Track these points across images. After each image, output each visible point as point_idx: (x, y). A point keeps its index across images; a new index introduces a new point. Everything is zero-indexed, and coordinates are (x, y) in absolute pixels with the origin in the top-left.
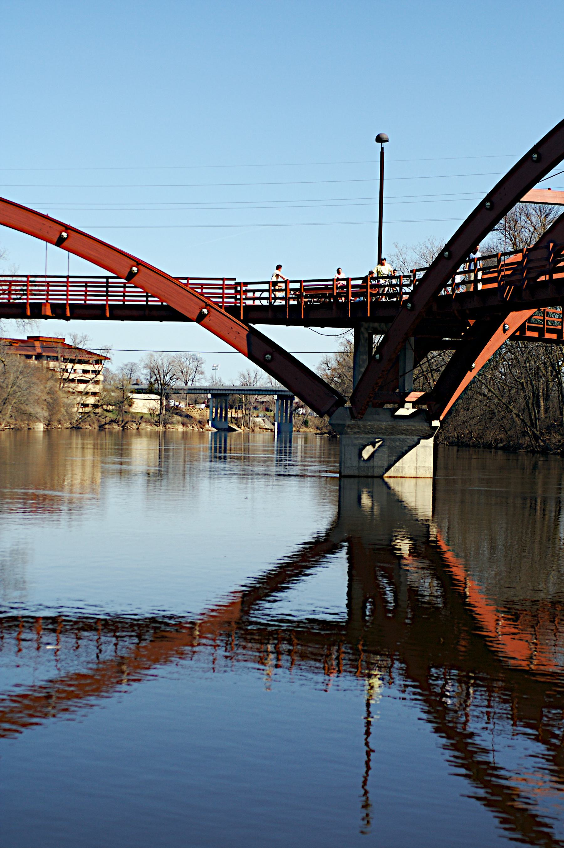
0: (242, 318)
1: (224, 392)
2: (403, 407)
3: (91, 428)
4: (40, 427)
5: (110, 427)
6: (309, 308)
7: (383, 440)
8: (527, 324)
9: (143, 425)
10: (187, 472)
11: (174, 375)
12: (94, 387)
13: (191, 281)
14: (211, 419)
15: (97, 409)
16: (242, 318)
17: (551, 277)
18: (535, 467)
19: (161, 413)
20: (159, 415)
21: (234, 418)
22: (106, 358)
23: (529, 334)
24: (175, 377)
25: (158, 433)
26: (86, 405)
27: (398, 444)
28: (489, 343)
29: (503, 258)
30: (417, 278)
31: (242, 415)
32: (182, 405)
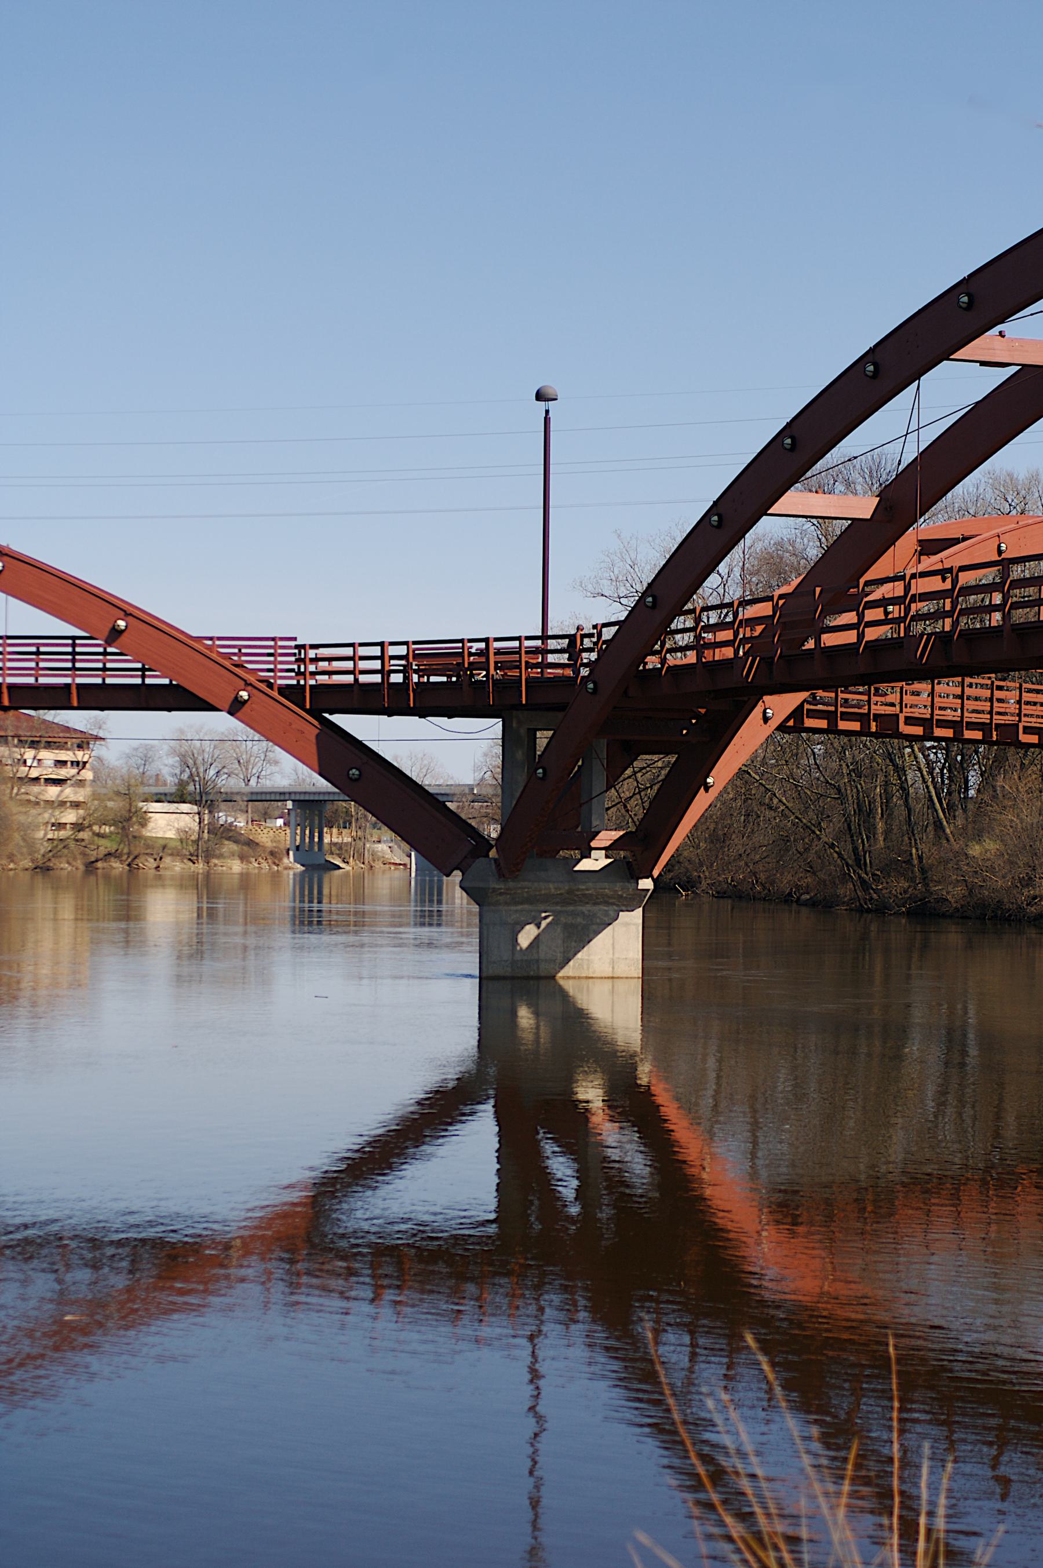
0: (308, 707)
1: (316, 798)
2: (589, 857)
3: (69, 868)
5: (105, 865)
7: (556, 914)
8: (806, 706)
11: (224, 767)
12: (76, 793)
14: (294, 848)
15: (81, 833)
16: (308, 707)
19: (199, 839)
20: (196, 842)
21: (335, 844)
22: (97, 738)
23: (809, 723)
24: (225, 770)
25: (194, 877)
26: (61, 826)
27: (579, 920)
30: (604, 638)
31: (350, 840)
32: (241, 823)
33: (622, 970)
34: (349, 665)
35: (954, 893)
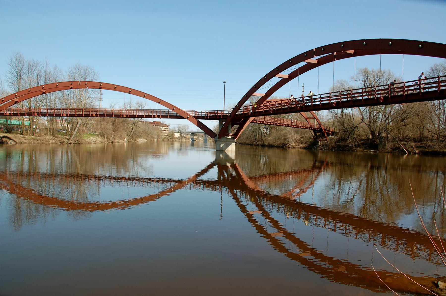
4: (156, 140)
6: (210, 116)
9: (177, 139)
10: (186, 149)
13: (186, 111)
17: (258, 111)
18: (256, 149)
20: (180, 137)
22: (169, 126)
23: (254, 122)
25: (180, 141)
26: (165, 135)
28: (246, 124)
29: (276, 102)
32: (185, 135)
33: (232, 150)
34: (201, 113)
35: (266, 144)
